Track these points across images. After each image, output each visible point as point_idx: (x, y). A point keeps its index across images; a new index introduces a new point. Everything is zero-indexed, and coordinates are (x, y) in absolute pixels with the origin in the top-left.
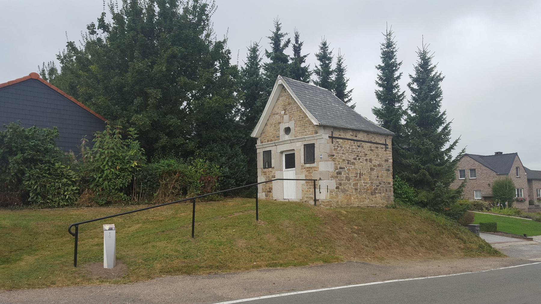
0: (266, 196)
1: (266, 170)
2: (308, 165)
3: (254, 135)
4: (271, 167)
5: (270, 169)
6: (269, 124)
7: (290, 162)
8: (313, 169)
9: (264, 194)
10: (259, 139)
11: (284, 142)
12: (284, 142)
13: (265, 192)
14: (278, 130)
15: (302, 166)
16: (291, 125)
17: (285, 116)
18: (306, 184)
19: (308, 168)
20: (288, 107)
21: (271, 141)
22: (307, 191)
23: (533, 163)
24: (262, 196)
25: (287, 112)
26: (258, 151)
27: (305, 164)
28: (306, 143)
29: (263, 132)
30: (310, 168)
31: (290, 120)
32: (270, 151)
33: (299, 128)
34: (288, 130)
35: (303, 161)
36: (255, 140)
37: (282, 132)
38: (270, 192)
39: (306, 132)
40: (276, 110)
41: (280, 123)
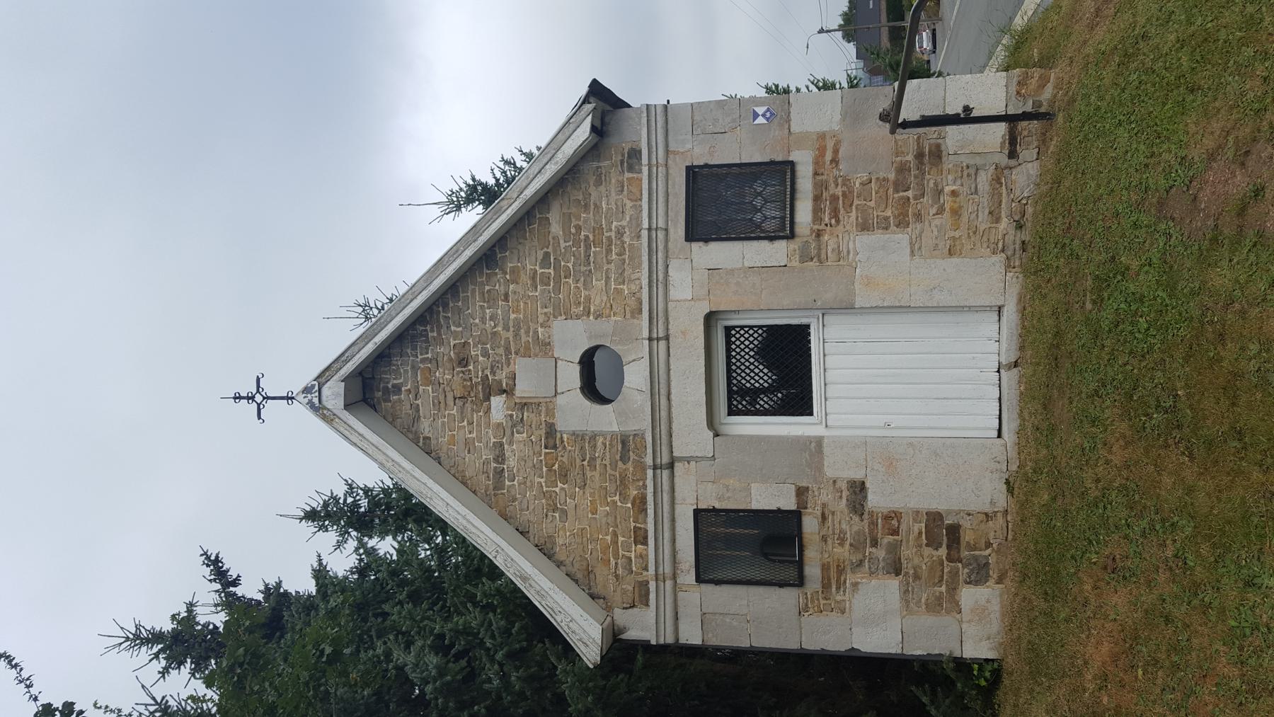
0: (980, 574)
1: (812, 571)
2: (804, 213)
3: (584, 631)
4: (795, 517)
5: (810, 525)
6: (546, 528)
7: (776, 368)
8: (829, 174)
9: (969, 596)
10: (621, 617)
11: (659, 388)
12: (659, 388)
13: (953, 589)
14: (585, 439)
15: (805, 257)
16: (571, 338)
17: (524, 389)
18: (915, 228)
19: (817, 217)
20: (480, 366)
21: (640, 504)
22: (956, 213)
23: (844, 5)
24: (981, 613)
25: (502, 376)
26: (691, 635)
27: (792, 236)
28: (679, 230)
29: (583, 582)
30: (817, 199)
31: (545, 347)
32: (699, 515)
33: (598, 284)
34: (596, 378)
35: (787, 598)
36: (620, 649)
37: (604, 419)
38: (954, 531)
39: (620, 233)
40: (476, 462)
41: (551, 431)
